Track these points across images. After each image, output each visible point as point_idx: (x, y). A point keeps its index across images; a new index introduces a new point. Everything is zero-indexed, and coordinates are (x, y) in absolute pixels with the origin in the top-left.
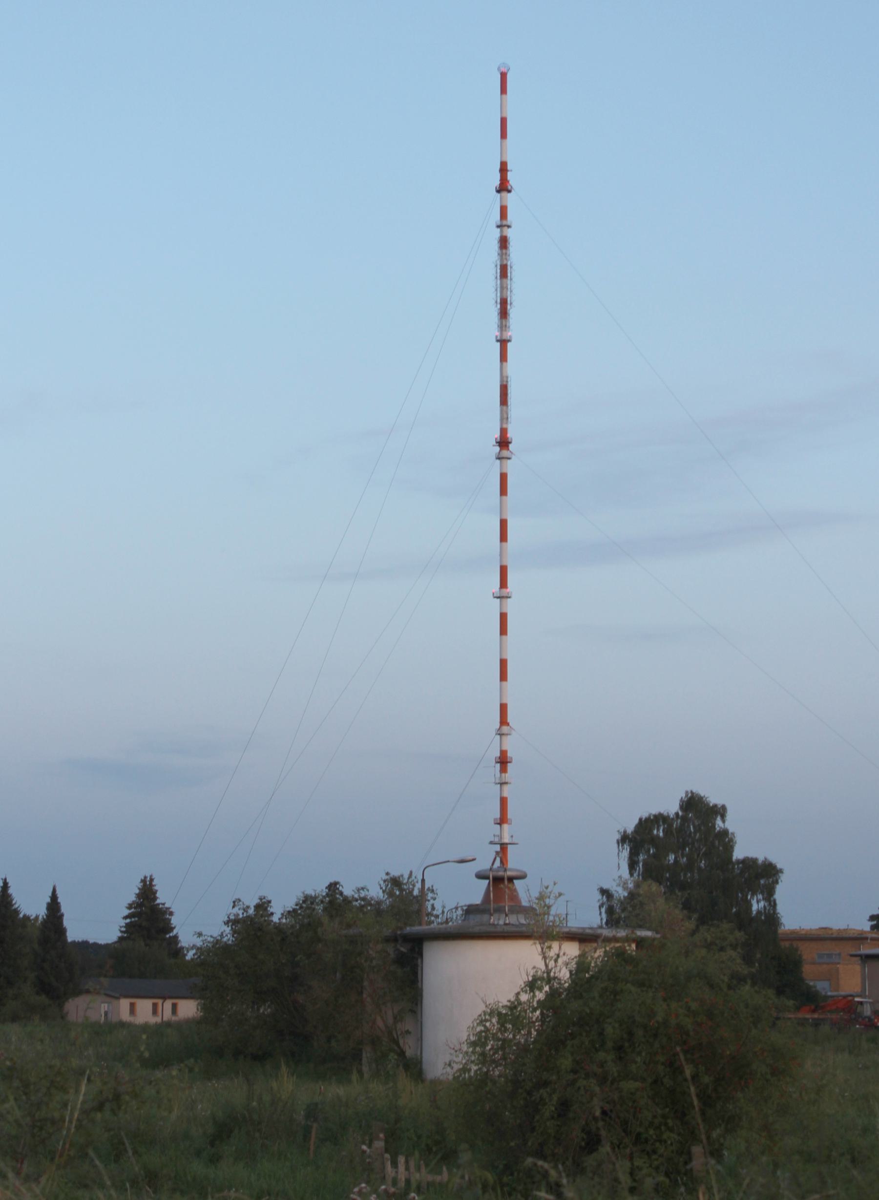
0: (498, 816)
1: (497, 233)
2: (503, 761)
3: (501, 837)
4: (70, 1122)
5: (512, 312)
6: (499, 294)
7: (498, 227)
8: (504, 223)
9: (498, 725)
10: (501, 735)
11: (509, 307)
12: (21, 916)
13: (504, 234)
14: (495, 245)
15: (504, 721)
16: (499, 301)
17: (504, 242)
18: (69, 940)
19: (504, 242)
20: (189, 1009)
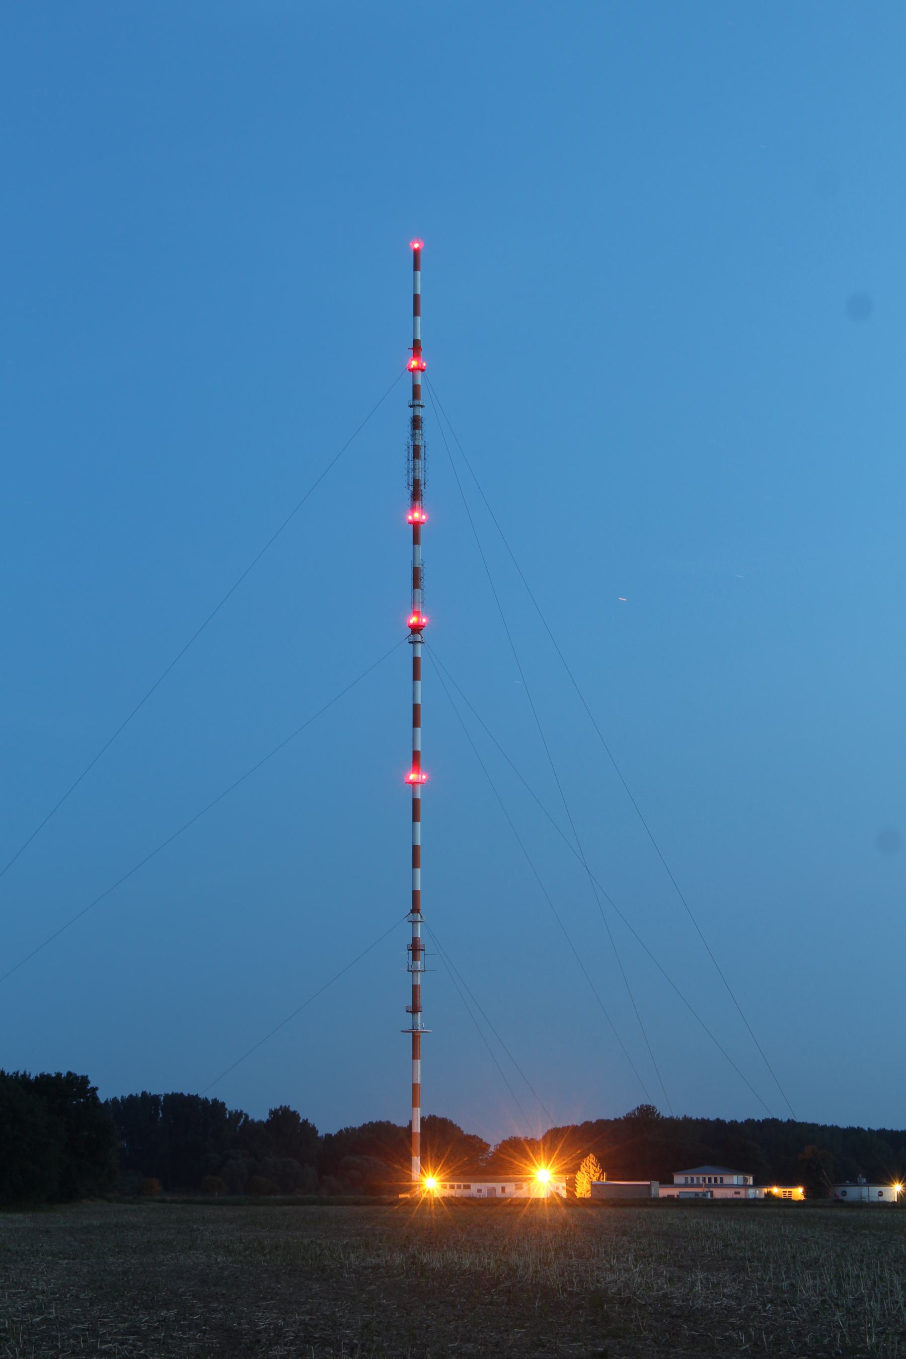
0: (410, 1004)
1: (410, 413)
2: (415, 948)
3: (414, 1024)
4: (357, 1203)
5: (425, 582)
6: (411, 476)
7: (411, 406)
8: (417, 402)
9: (411, 397)
10: (414, 643)
11: (422, 487)
12: (90, 1086)
13: (417, 414)
14: (408, 428)
15: (415, 910)
16: (411, 483)
17: (416, 422)
18: (102, 1100)
19: (416, 422)
20: (401, 1196)
